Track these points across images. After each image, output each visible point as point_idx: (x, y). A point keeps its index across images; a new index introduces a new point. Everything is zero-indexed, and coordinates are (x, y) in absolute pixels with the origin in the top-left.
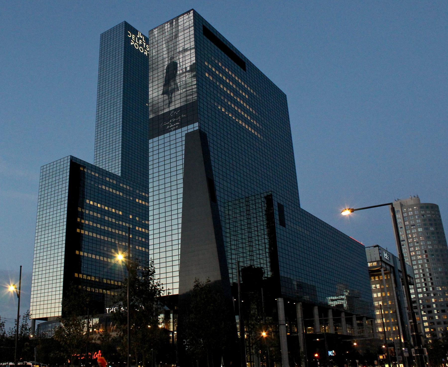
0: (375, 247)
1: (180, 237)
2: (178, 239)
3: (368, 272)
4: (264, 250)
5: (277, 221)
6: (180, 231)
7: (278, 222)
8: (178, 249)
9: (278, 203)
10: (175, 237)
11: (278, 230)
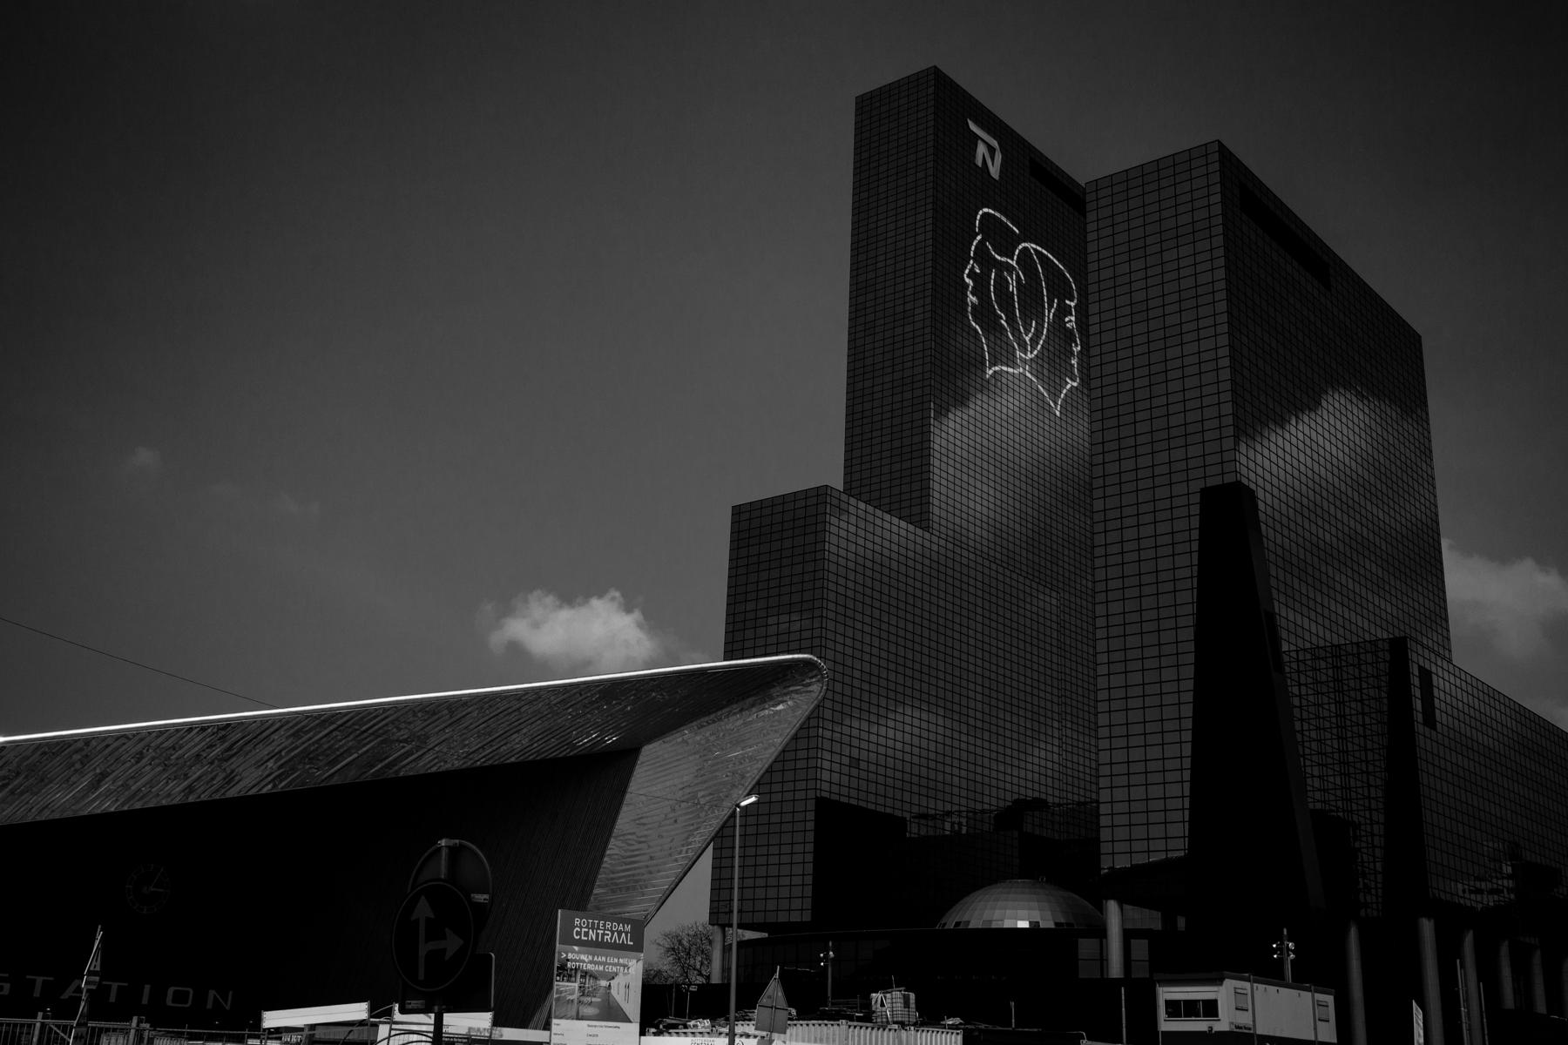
1: (1195, 562)
2: (1191, 552)
6: (1187, 775)
7: (1420, 718)
8: (1192, 589)
9: (1420, 667)
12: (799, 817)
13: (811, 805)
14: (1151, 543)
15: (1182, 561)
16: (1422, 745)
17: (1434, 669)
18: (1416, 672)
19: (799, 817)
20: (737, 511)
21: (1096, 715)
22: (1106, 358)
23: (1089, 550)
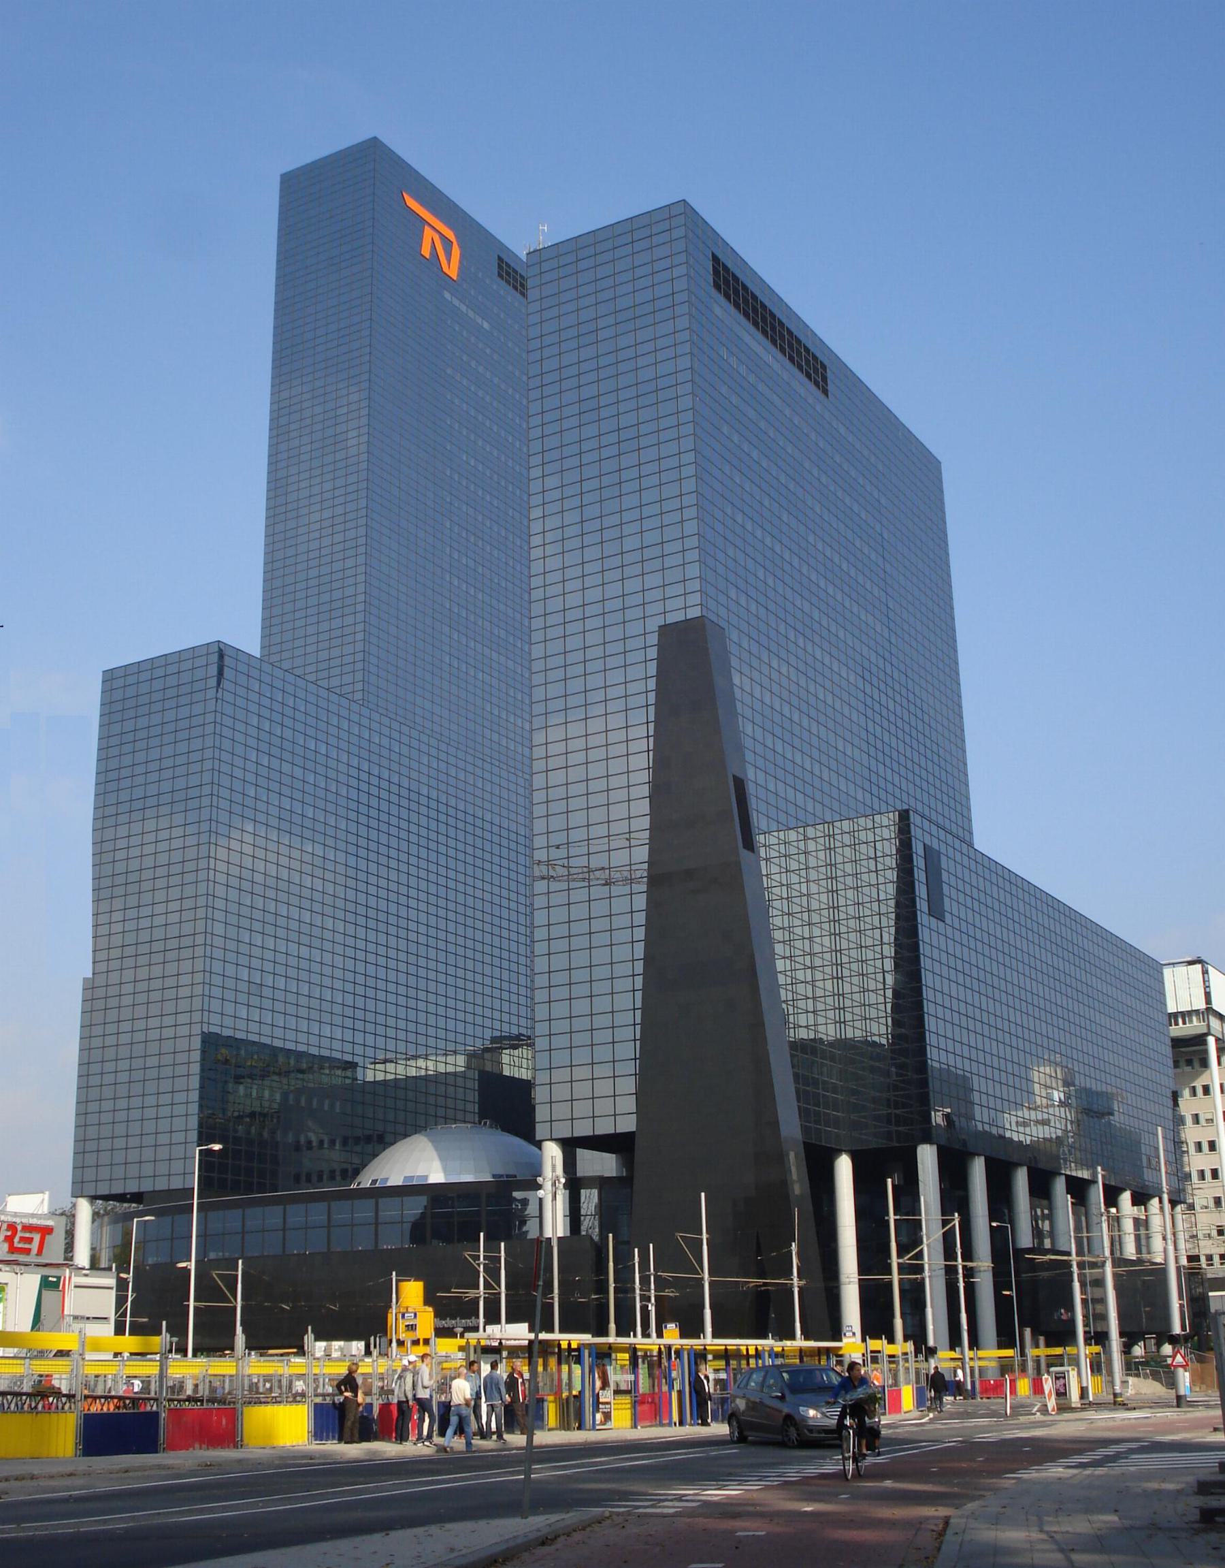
0: (1191, 963)
3: (1168, 1050)
4: (882, 992)
5: (922, 905)
7: (926, 909)
10: (622, 953)
11: (926, 931)
12: (182, 1058)
13: (197, 1043)
14: (598, 652)
15: (636, 672)
16: (927, 940)
17: (943, 850)
18: (921, 851)
19: (182, 1058)
20: (110, 677)
21: (533, 990)
22: (551, 591)
23: (527, 735)
